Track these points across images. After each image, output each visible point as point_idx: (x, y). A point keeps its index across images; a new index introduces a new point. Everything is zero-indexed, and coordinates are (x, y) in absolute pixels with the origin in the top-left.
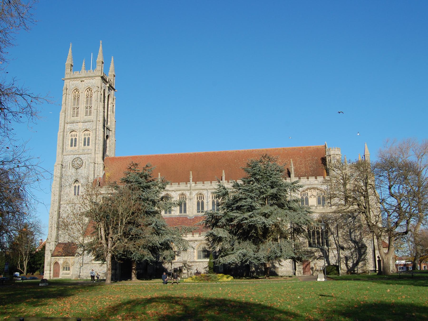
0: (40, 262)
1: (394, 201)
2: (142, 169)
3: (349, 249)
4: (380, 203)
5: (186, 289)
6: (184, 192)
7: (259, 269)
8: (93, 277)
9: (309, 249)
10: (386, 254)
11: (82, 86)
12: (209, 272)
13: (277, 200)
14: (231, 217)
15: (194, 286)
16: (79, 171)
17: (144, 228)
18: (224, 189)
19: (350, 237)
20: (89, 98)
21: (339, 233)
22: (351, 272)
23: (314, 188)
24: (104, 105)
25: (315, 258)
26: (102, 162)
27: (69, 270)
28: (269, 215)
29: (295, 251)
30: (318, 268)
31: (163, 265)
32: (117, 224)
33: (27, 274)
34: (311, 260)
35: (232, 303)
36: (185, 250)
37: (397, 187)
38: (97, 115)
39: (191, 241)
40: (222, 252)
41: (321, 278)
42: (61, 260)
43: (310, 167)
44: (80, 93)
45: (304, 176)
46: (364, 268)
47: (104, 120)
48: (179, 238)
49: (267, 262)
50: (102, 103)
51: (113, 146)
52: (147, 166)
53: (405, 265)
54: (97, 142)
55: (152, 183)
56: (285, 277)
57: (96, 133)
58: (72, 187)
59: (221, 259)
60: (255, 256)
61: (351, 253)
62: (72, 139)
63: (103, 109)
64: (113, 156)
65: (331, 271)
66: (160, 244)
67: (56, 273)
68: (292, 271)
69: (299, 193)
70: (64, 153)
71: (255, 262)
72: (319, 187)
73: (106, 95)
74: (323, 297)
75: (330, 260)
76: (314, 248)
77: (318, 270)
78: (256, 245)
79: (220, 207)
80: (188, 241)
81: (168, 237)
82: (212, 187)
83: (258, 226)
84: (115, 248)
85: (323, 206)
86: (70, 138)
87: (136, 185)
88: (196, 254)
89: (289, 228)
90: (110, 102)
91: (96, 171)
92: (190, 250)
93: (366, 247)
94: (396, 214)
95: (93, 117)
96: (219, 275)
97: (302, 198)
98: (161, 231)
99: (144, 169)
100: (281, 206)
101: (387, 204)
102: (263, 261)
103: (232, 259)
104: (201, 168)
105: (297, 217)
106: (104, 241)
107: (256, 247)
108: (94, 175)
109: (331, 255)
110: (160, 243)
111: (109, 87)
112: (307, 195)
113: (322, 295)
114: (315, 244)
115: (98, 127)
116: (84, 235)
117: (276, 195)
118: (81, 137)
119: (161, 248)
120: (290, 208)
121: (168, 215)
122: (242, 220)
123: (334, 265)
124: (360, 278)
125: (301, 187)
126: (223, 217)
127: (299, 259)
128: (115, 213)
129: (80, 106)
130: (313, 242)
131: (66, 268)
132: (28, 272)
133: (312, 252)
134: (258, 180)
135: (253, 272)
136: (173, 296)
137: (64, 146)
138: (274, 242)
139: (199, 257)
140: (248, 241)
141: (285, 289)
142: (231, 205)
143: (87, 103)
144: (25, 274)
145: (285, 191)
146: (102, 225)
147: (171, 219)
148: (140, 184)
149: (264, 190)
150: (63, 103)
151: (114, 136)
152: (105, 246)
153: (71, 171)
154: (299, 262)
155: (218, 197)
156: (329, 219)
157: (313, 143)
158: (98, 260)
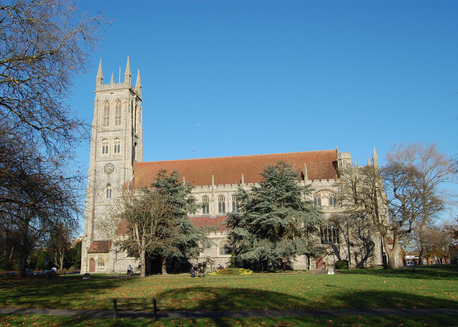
0: (74, 258)
2: (170, 175)
3: (358, 245)
6: (207, 194)
7: (276, 264)
9: (321, 245)
10: (391, 250)
11: (112, 98)
13: (292, 202)
17: (173, 227)
18: (243, 192)
19: (359, 235)
20: (118, 108)
21: (349, 231)
22: (360, 266)
24: (132, 115)
25: (327, 254)
26: (131, 167)
27: (104, 265)
28: (285, 216)
30: (329, 263)
31: (189, 261)
32: (149, 225)
35: (254, 291)
36: (209, 247)
37: (401, 190)
39: (214, 239)
41: (331, 272)
42: (96, 257)
43: (322, 170)
45: (317, 179)
46: (372, 263)
47: (133, 129)
48: (204, 236)
50: (131, 113)
51: (141, 152)
52: (174, 172)
53: (414, 260)
59: (242, 255)
62: (104, 147)
63: (131, 118)
64: (141, 161)
65: (341, 266)
67: (92, 268)
68: (306, 266)
69: (313, 196)
70: (97, 160)
71: (272, 257)
72: (331, 188)
73: (134, 106)
74: (329, 287)
75: (341, 255)
77: (329, 265)
78: (272, 242)
79: (240, 208)
80: (211, 239)
81: (194, 236)
83: (275, 225)
84: (148, 246)
85: (335, 206)
86: (102, 146)
87: (165, 190)
88: (218, 250)
90: (137, 112)
92: (213, 247)
93: (374, 244)
94: (400, 214)
95: (122, 126)
96: (240, 269)
97: (315, 199)
98: (188, 231)
99: (172, 175)
100: (295, 207)
101: (392, 204)
102: (280, 257)
103: (252, 255)
104: (223, 172)
106: (138, 240)
107: (273, 244)
109: (341, 251)
110: (187, 241)
111: (136, 98)
112: (320, 196)
113: (328, 286)
116: (117, 233)
117: (291, 197)
118: (111, 144)
119: (188, 245)
120: (304, 210)
122: (260, 221)
124: (366, 272)
126: (244, 217)
128: (148, 215)
129: (110, 116)
134: (274, 185)
135: (271, 267)
138: (289, 240)
139: (221, 253)
140: (266, 239)
141: (298, 281)
144: (61, 269)
145: (299, 194)
146: (136, 226)
147: (196, 219)
148: (169, 188)
150: (95, 113)
151: (141, 143)
152: (139, 244)
153: (103, 176)
154: (312, 258)
155: (239, 199)
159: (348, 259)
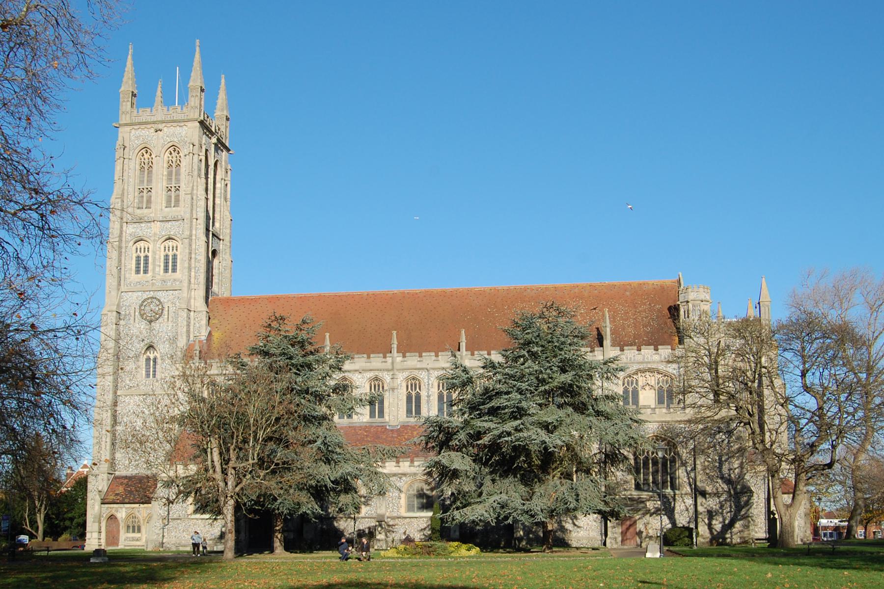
0: (70, 515)
1: (811, 403)
3: (717, 494)
4: (782, 405)
5: (388, 571)
6: (380, 374)
7: (533, 533)
8: (195, 545)
9: (635, 494)
10: (788, 507)
11: (159, 141)
12: (430, 538)
13: (572, 397)
14: (478, 429)
15: (403, 564)
16: (156, 325)
17: (300, 449)
18: (463, 371)
19: (720, 471)
20: (174, 167)
21: (698, 462)
22: (717, 541)
23: (651, 370)
24: (207, 184)
25: (648, 512)
26: (204, 308)
27: (139, 531)
28: (555, 427)
29: (608, 499)
30: (651, 532)
31: (336, 524)
33: (43, 539)
34: (638, 517)
36: (382, 493)
38: (192, 205)
39: (395, 475)
40: (459, 499)
41: (653, 553)
42: (122, 512)
44: (153, 156)
45: (631, 345)
46: (745, 534)
48: (371, 469)
49: (548, 520)
50: (204, 180)
51: (227, 274)
52: (304, 322)
53: (837, 528)
54: (193, 265)
55: (316, 357)
56: (583, 550)
57: (190, 245)
58: (141, 359)
59: (456, 512)
60: (525, 507)
61: (720, 502)
62: (138, 258)
63: (204, 193)
64: (227, 294)
65: (675, 540)
66: (332, 482)
67: (113, 538)
69: (621, 382)
70: (123, 288)
71: (525, 519)
72: (662, 367)
73: (211, 162)
75: (677, 516)
76: (646, 493)
78: (526, 485)
79: (455, 408)
81: (347, 468)
82: (437, 365)
83: (533, 448)
84: (242, 489)
85: (668, 407)
86: (135, 255)
87: (282, 362)
88: (403, 501)
89: (596, 451)
90: (218, 178)
91: (192, 327)
92: (392, 494)
93: (752, 492)
94: (812, 427)
95: (182, 210)
96: (451, 543)
97: (626, 391)
98: (335, 456)
100: (581, 408)
101: (796, 406)
102: (541, 517)
103: (478, 512)
104: (417, 324)
105: (611, 430)
106: (218, 476)
107: (527, 489)
108: (188, 336)
109: (679, 507)
110: (332, 479)
111: (216, 145)
112: (637, 384)
113: (644, 582)
114: (649, 485)
115: (194, 232)
116: (171, 458)
117: (571, 386)
118: (157, 252)
119: (334, 490)
120: (598, 413)
121: (345, 421)
122: (500, 436)
123: (684, 527)
125: (622, 370)
127: (614, 514)
128: (241, 419)
129: (153, 185)
130: (644, 480)
131: (134, 527)
132: (45, 534)
133: (640, 501)
134: (534, 356)
135: (520, 539)
136: (369, 582)
137: (123, 273)
138: (564, 481)
139: (410, 508)
140: (511, 478)
142: (479, 405)
143: (169, 179)
144: (40, 538)
145: (590, 377)
146: (214, 443)
148: (291, 358)
149: (546, 376)
150: (116, 178)
151: (228, 251)
152: (222, 484)
153: (138, 327)
154: (613, 520)
155: (453, 387)
156: (678, 435)
157: (652, 274)
158: (204, 513)
159: (692, 526)
